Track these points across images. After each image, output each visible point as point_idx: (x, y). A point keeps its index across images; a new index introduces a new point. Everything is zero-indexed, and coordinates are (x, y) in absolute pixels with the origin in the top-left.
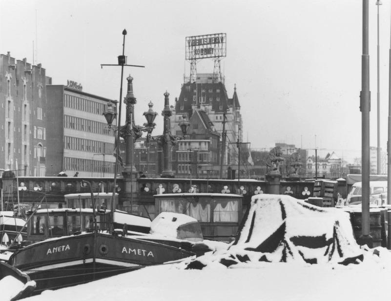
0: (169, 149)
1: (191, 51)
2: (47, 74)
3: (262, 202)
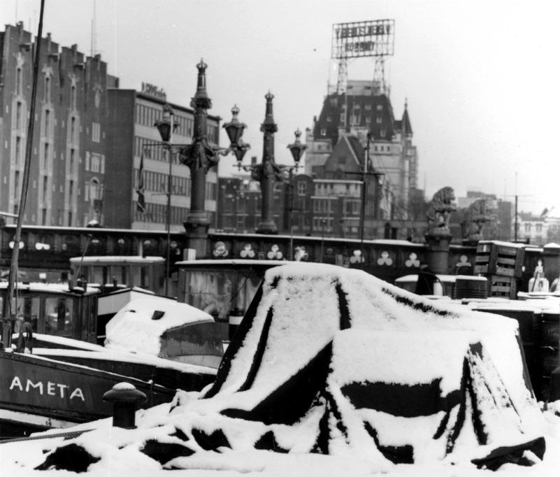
0: (270, 187)
1: (340, 45)
2: (111, 71)
3: (292, 286)
